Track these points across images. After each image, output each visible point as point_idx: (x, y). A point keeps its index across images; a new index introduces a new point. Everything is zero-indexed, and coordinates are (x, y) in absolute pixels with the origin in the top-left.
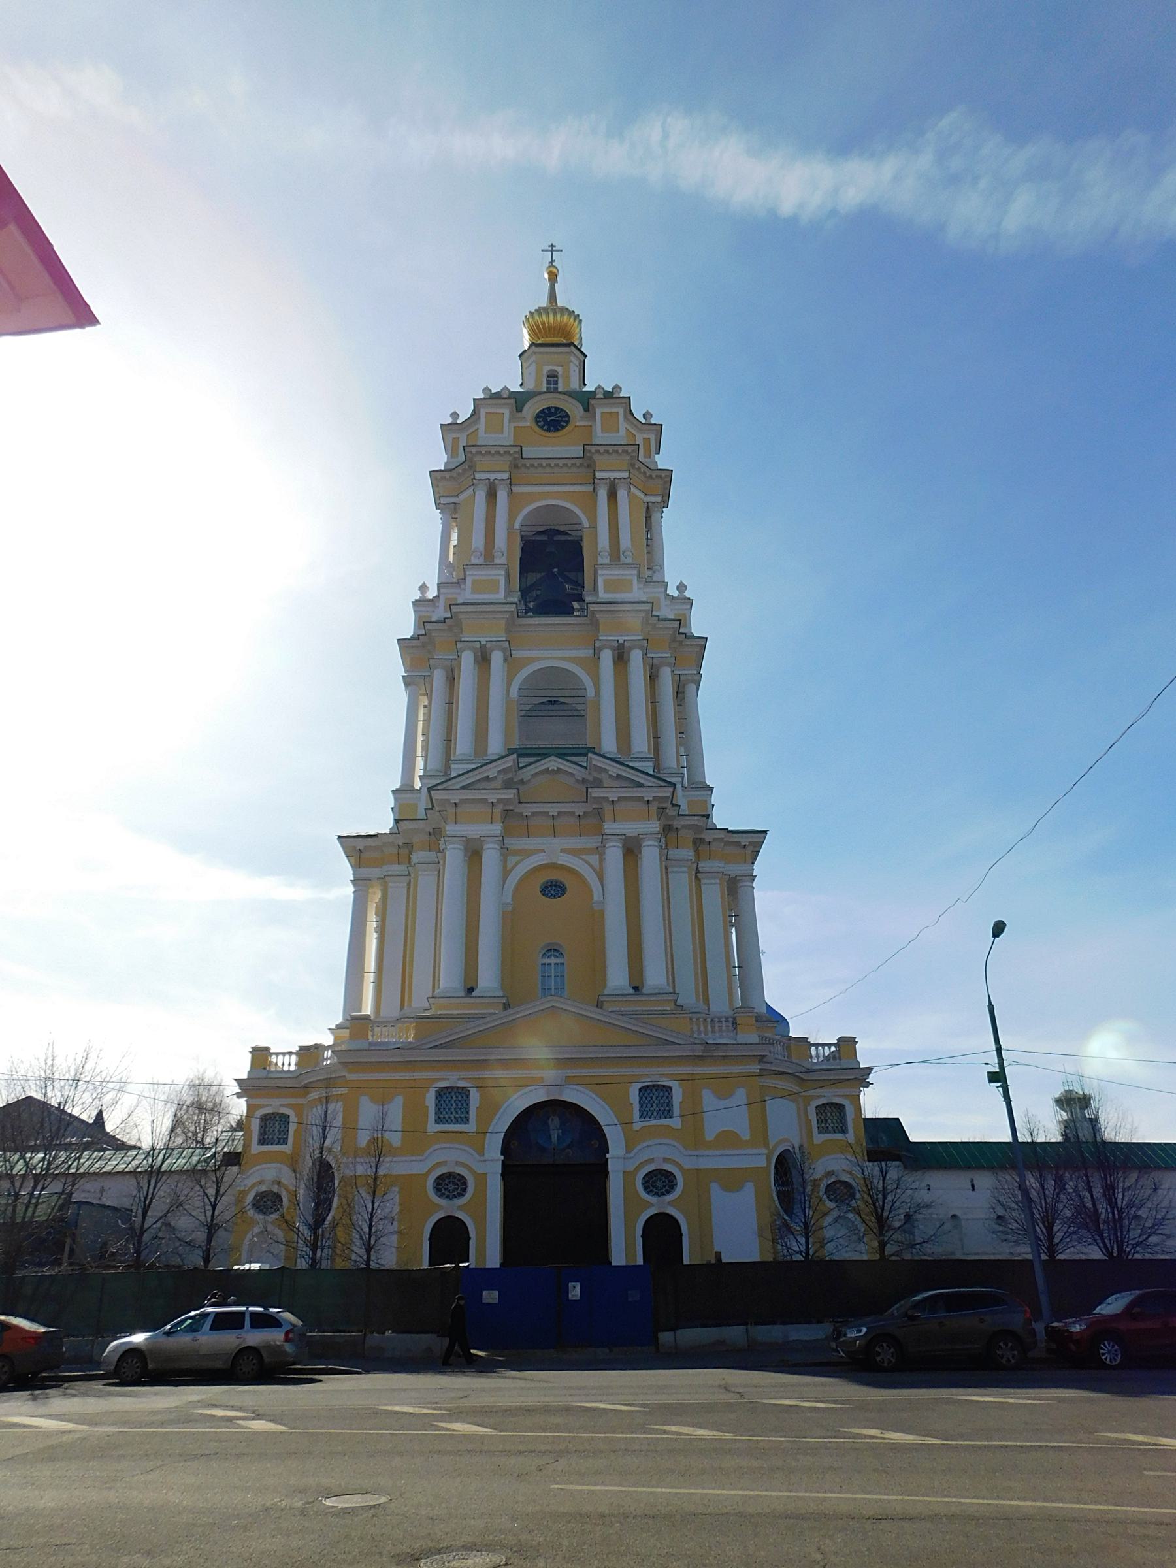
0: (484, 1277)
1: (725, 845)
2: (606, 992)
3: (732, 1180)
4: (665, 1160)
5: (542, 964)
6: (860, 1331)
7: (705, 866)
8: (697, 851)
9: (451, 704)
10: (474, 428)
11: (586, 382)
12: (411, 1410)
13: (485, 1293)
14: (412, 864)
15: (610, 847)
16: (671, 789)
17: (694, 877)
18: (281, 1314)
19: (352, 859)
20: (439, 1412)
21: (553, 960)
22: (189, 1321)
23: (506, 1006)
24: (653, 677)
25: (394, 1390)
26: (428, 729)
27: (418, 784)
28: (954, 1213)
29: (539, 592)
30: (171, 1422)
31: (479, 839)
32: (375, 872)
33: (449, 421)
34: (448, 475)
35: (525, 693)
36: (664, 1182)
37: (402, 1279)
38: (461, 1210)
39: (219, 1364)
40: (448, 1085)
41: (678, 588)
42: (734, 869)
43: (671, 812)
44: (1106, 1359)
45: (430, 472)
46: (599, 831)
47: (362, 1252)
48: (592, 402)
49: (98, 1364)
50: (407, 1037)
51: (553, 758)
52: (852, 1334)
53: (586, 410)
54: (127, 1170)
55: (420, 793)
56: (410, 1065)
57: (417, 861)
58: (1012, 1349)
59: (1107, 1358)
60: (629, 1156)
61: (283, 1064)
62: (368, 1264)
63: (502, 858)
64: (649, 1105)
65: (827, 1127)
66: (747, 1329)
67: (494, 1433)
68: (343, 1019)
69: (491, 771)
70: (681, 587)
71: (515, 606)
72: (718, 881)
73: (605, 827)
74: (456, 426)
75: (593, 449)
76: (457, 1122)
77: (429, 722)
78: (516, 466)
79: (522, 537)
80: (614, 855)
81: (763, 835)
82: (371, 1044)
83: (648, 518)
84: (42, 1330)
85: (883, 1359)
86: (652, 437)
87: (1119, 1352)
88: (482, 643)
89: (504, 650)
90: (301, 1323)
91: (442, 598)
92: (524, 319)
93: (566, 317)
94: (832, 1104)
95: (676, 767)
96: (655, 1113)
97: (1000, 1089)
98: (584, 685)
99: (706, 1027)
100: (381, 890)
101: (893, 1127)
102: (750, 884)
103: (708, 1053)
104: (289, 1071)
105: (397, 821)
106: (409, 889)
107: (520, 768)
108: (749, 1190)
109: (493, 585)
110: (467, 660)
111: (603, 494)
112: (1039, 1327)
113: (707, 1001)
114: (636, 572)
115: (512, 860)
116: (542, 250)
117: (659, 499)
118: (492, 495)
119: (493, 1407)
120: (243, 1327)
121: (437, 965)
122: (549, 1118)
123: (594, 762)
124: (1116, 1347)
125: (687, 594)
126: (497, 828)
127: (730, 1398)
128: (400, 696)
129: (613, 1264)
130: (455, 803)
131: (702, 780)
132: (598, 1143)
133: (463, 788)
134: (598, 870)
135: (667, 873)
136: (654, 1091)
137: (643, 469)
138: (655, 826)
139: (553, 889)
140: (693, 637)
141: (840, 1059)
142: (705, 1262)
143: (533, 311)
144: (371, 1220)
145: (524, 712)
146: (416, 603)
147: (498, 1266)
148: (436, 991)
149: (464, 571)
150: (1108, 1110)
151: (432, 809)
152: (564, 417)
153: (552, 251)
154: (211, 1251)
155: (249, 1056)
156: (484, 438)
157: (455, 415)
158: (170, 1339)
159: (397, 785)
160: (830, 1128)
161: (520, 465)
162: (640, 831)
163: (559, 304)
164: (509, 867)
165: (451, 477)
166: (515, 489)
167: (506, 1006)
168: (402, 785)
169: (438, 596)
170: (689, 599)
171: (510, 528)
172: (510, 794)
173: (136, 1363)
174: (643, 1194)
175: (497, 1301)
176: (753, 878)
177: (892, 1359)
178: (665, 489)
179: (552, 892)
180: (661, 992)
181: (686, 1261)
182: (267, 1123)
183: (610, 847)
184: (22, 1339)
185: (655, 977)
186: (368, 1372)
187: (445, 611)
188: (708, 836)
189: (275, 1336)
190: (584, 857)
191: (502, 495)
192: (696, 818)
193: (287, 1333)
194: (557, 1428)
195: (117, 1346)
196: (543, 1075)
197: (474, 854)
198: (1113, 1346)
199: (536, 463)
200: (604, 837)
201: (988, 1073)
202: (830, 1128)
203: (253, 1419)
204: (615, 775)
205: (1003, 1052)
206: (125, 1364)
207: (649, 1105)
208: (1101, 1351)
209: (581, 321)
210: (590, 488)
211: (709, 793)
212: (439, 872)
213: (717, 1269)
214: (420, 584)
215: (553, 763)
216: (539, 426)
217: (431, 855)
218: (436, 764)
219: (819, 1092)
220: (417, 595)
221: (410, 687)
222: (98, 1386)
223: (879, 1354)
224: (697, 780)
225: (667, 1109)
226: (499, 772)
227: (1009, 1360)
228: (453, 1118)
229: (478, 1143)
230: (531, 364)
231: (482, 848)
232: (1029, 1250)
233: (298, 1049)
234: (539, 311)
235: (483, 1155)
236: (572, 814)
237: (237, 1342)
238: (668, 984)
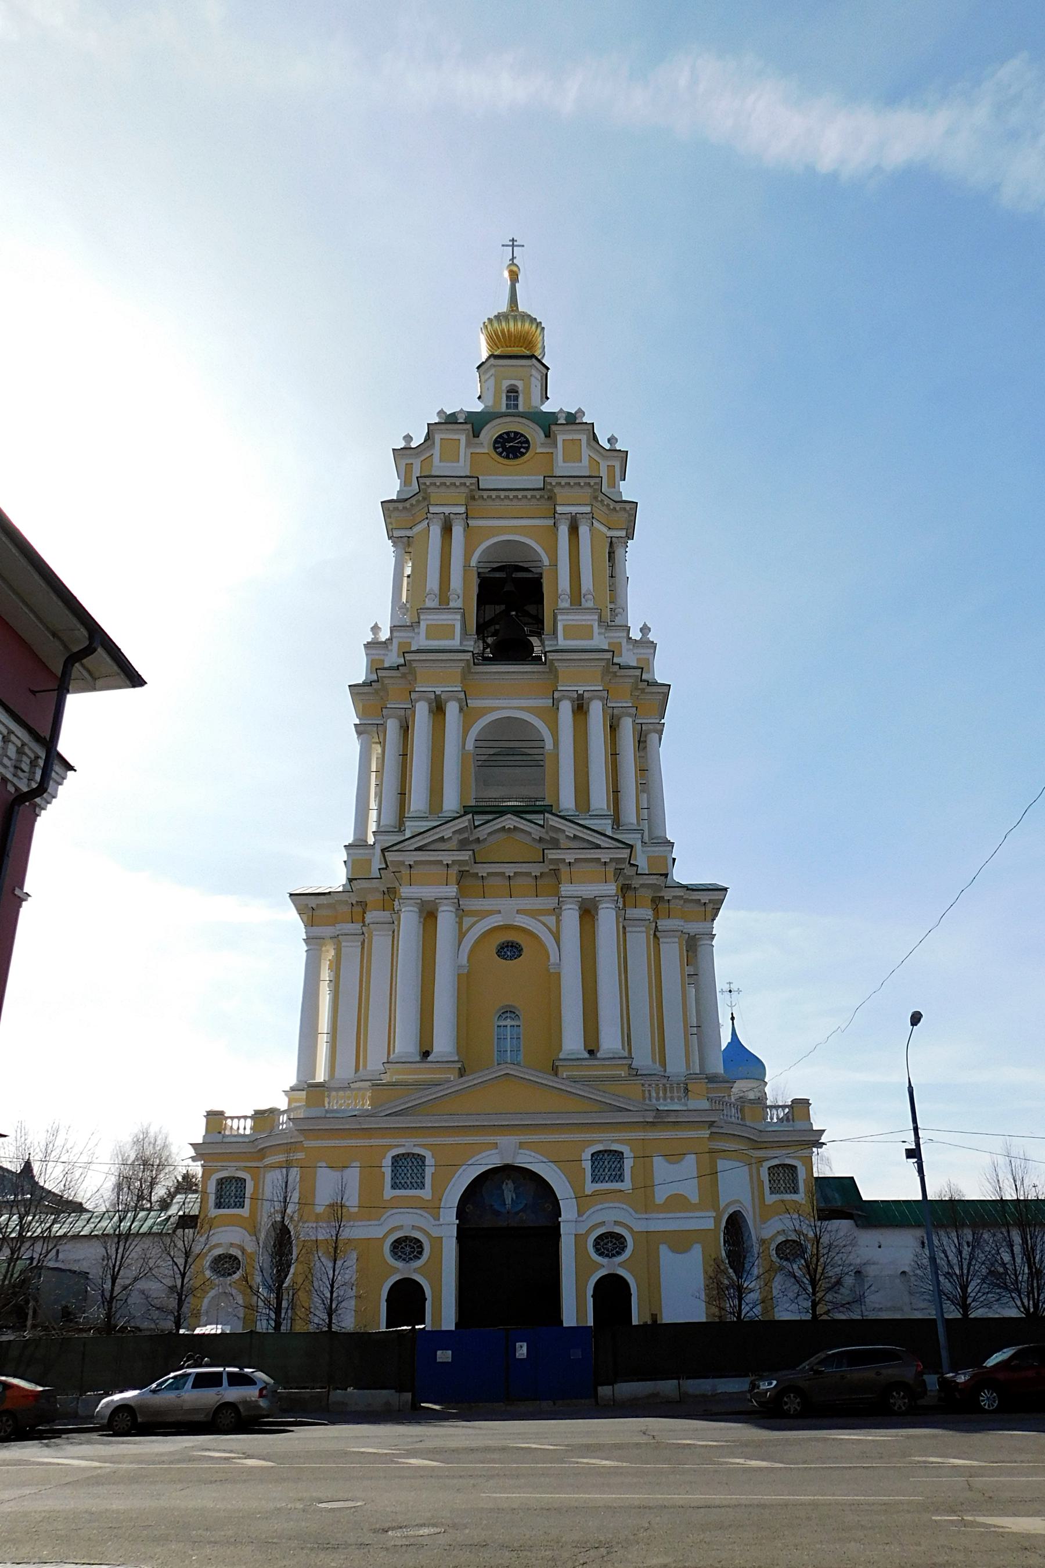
0: (439, 1338)
1: (684, 902)
2: (561, 1056)
3: (680, 1242)
4: (616, 1223)
5: (498, 1026)
6: (771, 1384)
7: (664, 924)
8: (656, 910)
9: (405, 756)
10: (428, 455)
11: (548, 396)
12: (375, 1451)
13: (439, 1353)
14: (366, 923)
15: (565, 910)
16: (629, 851)
17: (652, 937)
18: (255, 1373)
19: (305, 917)
20: (398, 1452)
21: (509, 1022)
22: (171, 1381)
23: (462, 1073)
24: (613, 727)
25: (357, 1437)
26: (383, 766)
27: (371, 840)
28: (901, 1271)
29: (497, 627)
30: (179, 1461)
31: (434, 901)
32: (328, 931)
33: (402, 444)
34: (400, 506)
35: (480, 744)
36: (615, 1244)
37: (360, 1340)
38: (417, 1273)
39: (201, 1417)
40: (404, 1152)
41: (641, 630)
42: (693, 928)
43: (631, 872)
44: (985, 1405)
45: (382, 502)
47: (325, 1317)
48: (554, 428)
49: (91, 1418)
50: (363, 1105)
51: (509, 816)
52: (764, 1386)
54: (82, 1234)
55: (374, 848)
56: (367, 1132)
57: (371, 921)
58: (904, 1397)
59: (985, 1404)
60: (581, 1219)
61: (238, 1128)
62: (330, 1325)
63: (457, 919)
64: (601, 1170)
65: (779, 1188)
66: (679, 1383)
67: (442, 1465)
68: (298, 1080)
69: (447, 832)
70: (645, 629)
71: (471, 654)
72: (677, 940)
73: (562, 889)
74: (408, 452)
75: (554, 481)
76: (413, 1187)
77: (382, 774)
78: (473, 498)
79: (479, 574)
80: (571, 917)
81: (724, 892)
82: (327, 1111)
83: (611, 554)
84: (40, 1389)
85: (790, 1407)
86: (617, 465)
87: (997, 1398)
88: (437, 693)
89: (459, 700)
90: (273, 1381)
91: (395, 642)
92: (482, 326)
93: (527, 325)
94: (785, 1165)
95: (635, 822)
96: (607, 1178)
97: (916, 1164)
98: (542, 736)
99: (658, 1094)
100: (334, 949)
101: (848, 1185)
102: (709, 942)
103: (660, 1120)
104: (244, 1135)
105: (350, 880)
106: (363, 948)
107: (476, 827)
108: (697, 1251)
109: (446, 631)
110: (422, 711)
111: (564, 530)
112: (931, 1380)
113: (663, 1064)
114: (596, 617)
115: (467, 921)
116: (503, 245)
118: (447, 529)
119: (443, 1448)
120: (221, 1385)
121: (392, 1016)
122: (503, 1183)
123: (551, 823)
124: (995, 1394)
125: (651, 637)
126: (452, 890)
127: (643, 1440)
128: (353, 745)
129: (565, 1325)
130: (410, 865)
131: (663, 835)
132: (551, 1207)
133: (416, 850)
135: (624, 933)
136: (606, 1155)
137: (607, 501)
138: (612, 888)
139: (510, 950)
140: (656, 684)
141: (793, 1121)
142: (642, 1323)
143: (492, 317)
144: (332, 1286)
145: (480, 762)
146: (368, 646)
147: (453, 1328)
148: (392, 1056)
149: (418, 614)
150: (1031, 1177)
151: (386, 869)
152: (524, 442)
153: (513, 246)
154: (182, 1316)
155: (204, 1120)
156: (439, 467)
157: (408, 438)
158: (156, 1396)
159: (350, 840)
160: (782, 1188)
161: (476, 497)
162: (596, 893)
163: (520, 309)
164: (464, 930)
165: (405, 508)
166: (471, 522)
167: (462, 1073)
168: (355, 840)
169: (390, 639)
170: (652, 642)
171: (466, 566)
172: (465, 856)
173: (127, 1417)
174: (595, 1257)
175: (450, 1360)
177: (797, 1407)
178: (629, 521)
179: (509, 954)
180: (616, 1056)
181: (635, 1322)
182: (224, 1186)
183: (565, 910)
184: (23, 1396)
185: (610, 1041)
186: (333, 1423)
187: (398, 656)
188: (667, 894)
189: (251, 1393)
191: (458, 530)
192: (655, 877)
193: (261, 1390)
194: (494, 1461)
195: (108, 1404)
196: (498, 1141)
197: (429, 914)
198: (992, 1394)
199: (494, 494)
200: (561, 899)
201: (906, 1150)
202: (782, 1188)
203: (246, 1458)
204: (572, 836)
205: (919, 1131)
206: (117, 1418)
207: (601, 1170)
208: (982, 1398)
209: (543, 328)
210: (551, 522)
211: (670, 848)
212: (393, 932)
213: (655, 1328)
214: (373, 625)
215: (510, 822)
216: (497, 452)
217: (385, 916)
218: (390, 819)
219: (770, 1153)
220: (370, 637)
221: (362, 736)
222: (94, 1436)
223: (786, 1403)
224: (659, 835)
225: (619, 1173)
226: (454, 833)
227: (900, 1408)
228: (409, 1183)
229: (434, 1209)
230: (489, 378)
231: (437, 910)
232: (934, 1312)
233: (253, 1113)
234: (498, 317)
235: (439, 1220)
236: (528, 874)
237: (217, 1398)
238: (623, 1048)
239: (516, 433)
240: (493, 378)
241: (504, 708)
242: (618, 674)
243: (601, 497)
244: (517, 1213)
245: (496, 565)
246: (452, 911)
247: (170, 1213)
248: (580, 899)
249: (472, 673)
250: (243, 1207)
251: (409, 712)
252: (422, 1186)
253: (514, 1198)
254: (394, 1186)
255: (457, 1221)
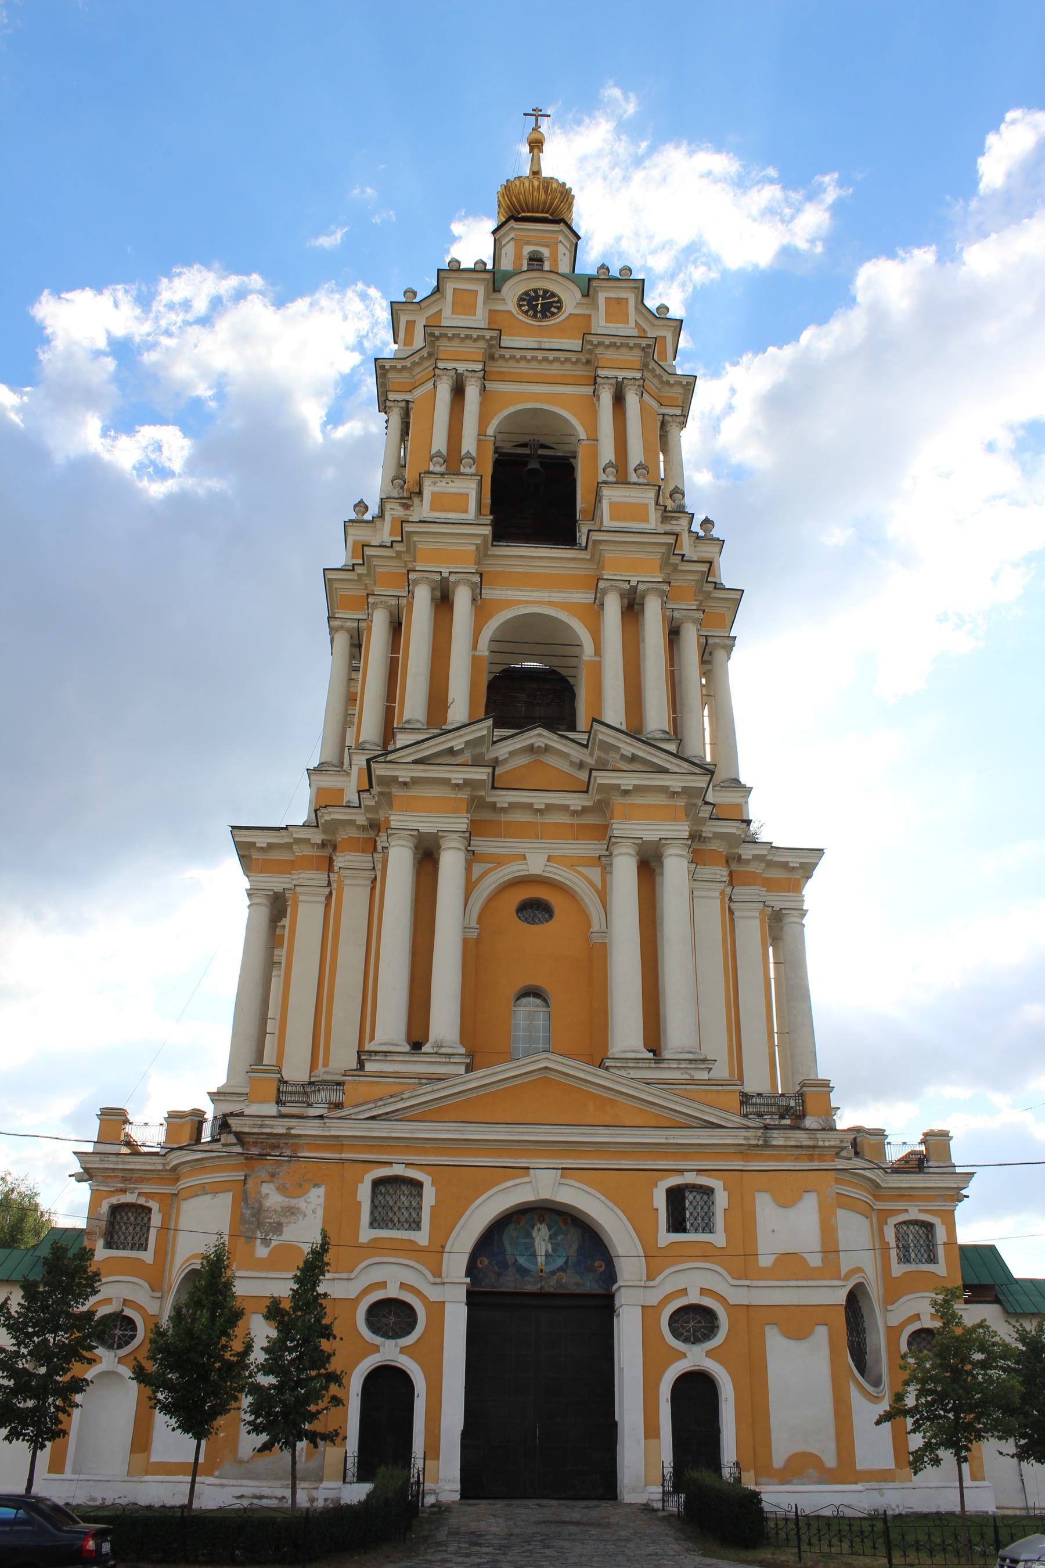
4: (704, 1291)
15: (620, 854)
16: (708, 778)
24: (674, 633)
42: (778, 900)
46: (603, 832)
53: (586, 294)
73: (614, 826)
78: (492, 357)
102: (797, 920)
106: (328, 905)
107: (494, 743)
108: (821, 1333)
109: (458, 502)
111: (606, 398)
115: (477, 870)
116: (525, 114)
117: (678, 412)
118: (458, 392)
122: (533, 1228)
125: (715, 533)
132: (604, 1266)
133: (416, 762)
134: (599, 887)
151: (368, 791)
159: (314, 763)
161: (497, 356)
162: (664, 835)
164: (474, 878)
166: (488, 385)
167: (470, 1068)
170: (718, 539)
171: (482, 433)
172: (482, 774)
176: (803, 913)
190: (579, 869)
191: (472, 392)
199: (518, 354)
200: (613, 840)
210: (589, 390)
216: (522, 311)
231: (439, 847)
239: (546, 292)
240: (512, 242)
241: (528, 602)
242: (680, 568)
243: (652, 365)
244: (553, 1273)
245: (517, 443)
246: (459, 849)
247: (493, 1551)
248: (640, 841)
249: (489, 556)
250: (146, 1249)
251: (363, 625)
252: (416, 1225)
253: (550, 1250)
254: (374, 1223)
255: (468, 1280)
